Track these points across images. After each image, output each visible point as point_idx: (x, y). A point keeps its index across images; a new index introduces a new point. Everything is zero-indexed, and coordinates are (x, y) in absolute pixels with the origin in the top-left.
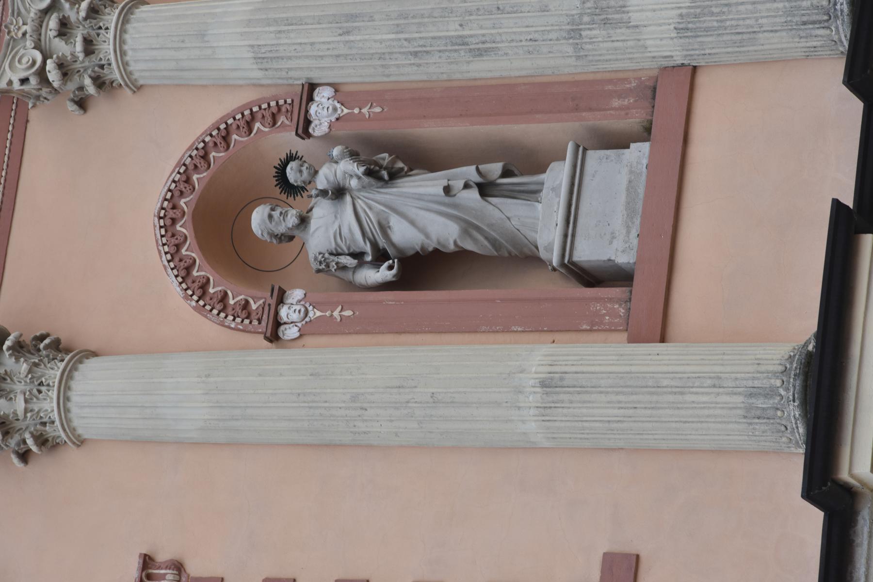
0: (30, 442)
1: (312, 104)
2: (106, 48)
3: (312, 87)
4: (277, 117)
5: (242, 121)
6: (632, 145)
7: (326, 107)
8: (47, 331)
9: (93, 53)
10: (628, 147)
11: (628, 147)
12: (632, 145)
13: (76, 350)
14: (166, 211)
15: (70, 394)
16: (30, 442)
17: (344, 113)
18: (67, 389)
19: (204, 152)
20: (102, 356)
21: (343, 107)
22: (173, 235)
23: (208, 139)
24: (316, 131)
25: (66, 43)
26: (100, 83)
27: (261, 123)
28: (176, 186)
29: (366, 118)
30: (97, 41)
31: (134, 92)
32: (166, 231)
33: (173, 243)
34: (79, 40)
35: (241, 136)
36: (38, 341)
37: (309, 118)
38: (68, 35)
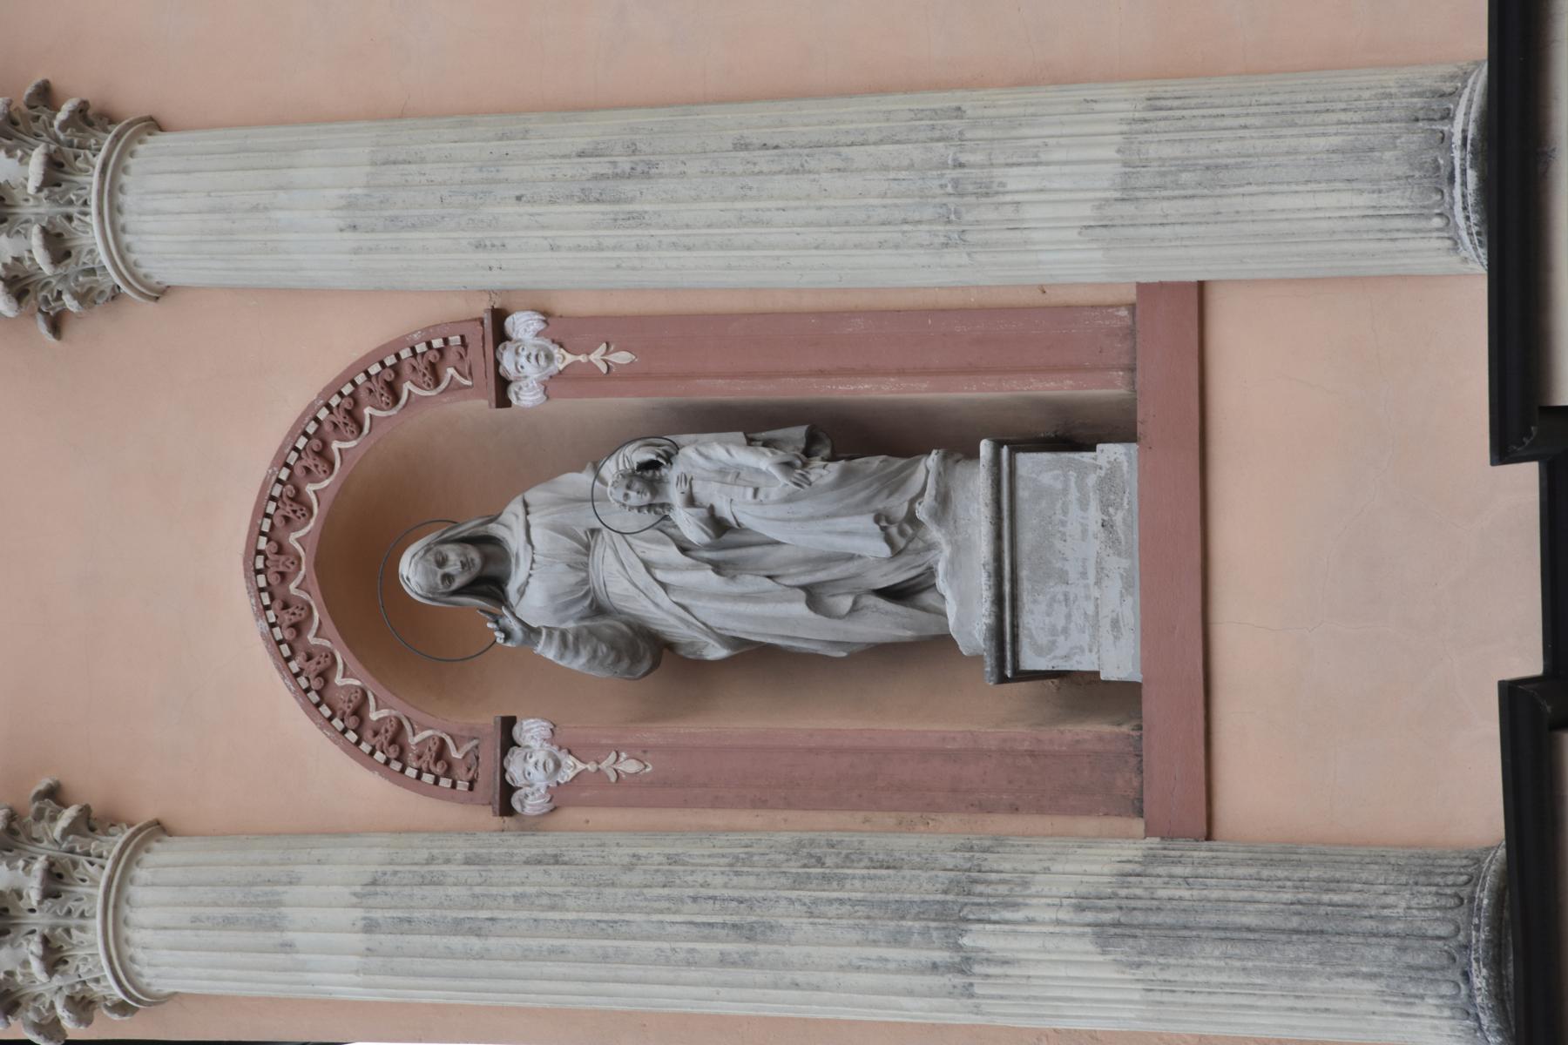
0: (61, 1011)
1: (505, 348)
2: (91, 238)
3: (499, 316)
4: (440, 368)
5: (378, 383)
6: (1099, 447)
7: (534, 353)
8: (56, 779)
9: (68, 254)
10: (1093, 449)
11: (1093, 449)
12: (1099, 447)
13: (120, 122)
14: (266, 558)
15: (121, 198)
16: (61, 1011)
17: (566, 363)
18: (119, 232)
19: (320, 444)
20: (181, 835)
21: (562, 351)
22: (286, 606)
23: (323, 414)
24: (528, 807)
25: (8, 236)
26: (84, 297)
27: (412, 382)
28: (277, 508)
29: (610, 782)
30: (72, 877)
31: (157, 298)
32: (272, 598)
33: (287, 623)
34: (38, 866)
35: (381, 409)
36: (46, 800)
37: (511, 782)
38: (10, 219)
